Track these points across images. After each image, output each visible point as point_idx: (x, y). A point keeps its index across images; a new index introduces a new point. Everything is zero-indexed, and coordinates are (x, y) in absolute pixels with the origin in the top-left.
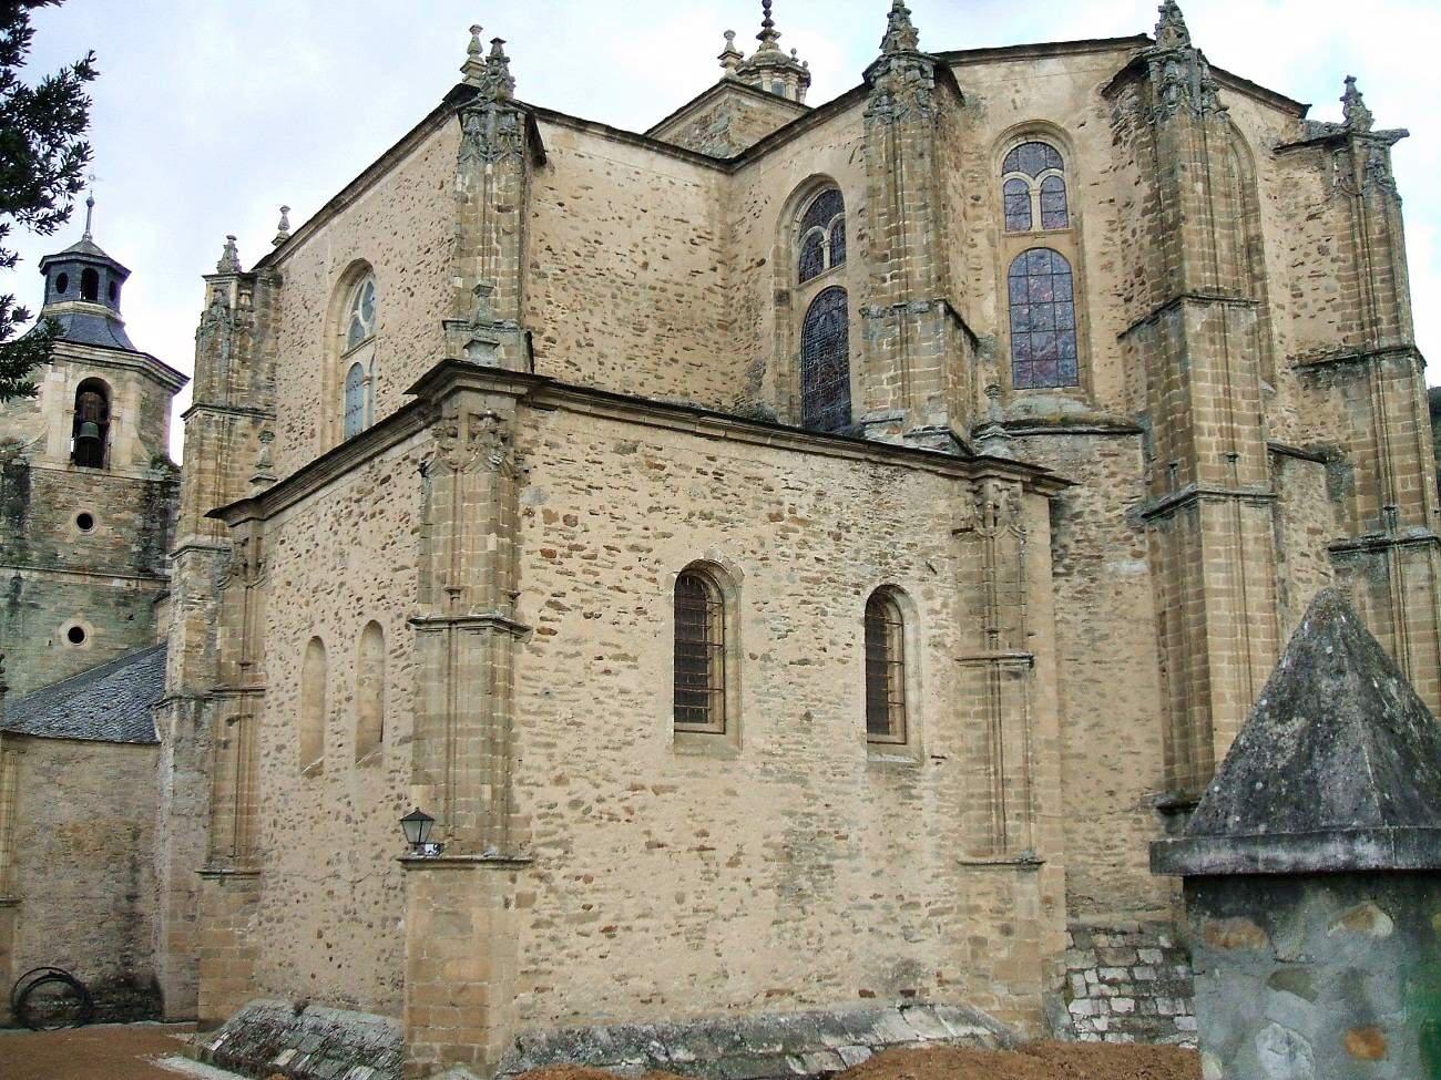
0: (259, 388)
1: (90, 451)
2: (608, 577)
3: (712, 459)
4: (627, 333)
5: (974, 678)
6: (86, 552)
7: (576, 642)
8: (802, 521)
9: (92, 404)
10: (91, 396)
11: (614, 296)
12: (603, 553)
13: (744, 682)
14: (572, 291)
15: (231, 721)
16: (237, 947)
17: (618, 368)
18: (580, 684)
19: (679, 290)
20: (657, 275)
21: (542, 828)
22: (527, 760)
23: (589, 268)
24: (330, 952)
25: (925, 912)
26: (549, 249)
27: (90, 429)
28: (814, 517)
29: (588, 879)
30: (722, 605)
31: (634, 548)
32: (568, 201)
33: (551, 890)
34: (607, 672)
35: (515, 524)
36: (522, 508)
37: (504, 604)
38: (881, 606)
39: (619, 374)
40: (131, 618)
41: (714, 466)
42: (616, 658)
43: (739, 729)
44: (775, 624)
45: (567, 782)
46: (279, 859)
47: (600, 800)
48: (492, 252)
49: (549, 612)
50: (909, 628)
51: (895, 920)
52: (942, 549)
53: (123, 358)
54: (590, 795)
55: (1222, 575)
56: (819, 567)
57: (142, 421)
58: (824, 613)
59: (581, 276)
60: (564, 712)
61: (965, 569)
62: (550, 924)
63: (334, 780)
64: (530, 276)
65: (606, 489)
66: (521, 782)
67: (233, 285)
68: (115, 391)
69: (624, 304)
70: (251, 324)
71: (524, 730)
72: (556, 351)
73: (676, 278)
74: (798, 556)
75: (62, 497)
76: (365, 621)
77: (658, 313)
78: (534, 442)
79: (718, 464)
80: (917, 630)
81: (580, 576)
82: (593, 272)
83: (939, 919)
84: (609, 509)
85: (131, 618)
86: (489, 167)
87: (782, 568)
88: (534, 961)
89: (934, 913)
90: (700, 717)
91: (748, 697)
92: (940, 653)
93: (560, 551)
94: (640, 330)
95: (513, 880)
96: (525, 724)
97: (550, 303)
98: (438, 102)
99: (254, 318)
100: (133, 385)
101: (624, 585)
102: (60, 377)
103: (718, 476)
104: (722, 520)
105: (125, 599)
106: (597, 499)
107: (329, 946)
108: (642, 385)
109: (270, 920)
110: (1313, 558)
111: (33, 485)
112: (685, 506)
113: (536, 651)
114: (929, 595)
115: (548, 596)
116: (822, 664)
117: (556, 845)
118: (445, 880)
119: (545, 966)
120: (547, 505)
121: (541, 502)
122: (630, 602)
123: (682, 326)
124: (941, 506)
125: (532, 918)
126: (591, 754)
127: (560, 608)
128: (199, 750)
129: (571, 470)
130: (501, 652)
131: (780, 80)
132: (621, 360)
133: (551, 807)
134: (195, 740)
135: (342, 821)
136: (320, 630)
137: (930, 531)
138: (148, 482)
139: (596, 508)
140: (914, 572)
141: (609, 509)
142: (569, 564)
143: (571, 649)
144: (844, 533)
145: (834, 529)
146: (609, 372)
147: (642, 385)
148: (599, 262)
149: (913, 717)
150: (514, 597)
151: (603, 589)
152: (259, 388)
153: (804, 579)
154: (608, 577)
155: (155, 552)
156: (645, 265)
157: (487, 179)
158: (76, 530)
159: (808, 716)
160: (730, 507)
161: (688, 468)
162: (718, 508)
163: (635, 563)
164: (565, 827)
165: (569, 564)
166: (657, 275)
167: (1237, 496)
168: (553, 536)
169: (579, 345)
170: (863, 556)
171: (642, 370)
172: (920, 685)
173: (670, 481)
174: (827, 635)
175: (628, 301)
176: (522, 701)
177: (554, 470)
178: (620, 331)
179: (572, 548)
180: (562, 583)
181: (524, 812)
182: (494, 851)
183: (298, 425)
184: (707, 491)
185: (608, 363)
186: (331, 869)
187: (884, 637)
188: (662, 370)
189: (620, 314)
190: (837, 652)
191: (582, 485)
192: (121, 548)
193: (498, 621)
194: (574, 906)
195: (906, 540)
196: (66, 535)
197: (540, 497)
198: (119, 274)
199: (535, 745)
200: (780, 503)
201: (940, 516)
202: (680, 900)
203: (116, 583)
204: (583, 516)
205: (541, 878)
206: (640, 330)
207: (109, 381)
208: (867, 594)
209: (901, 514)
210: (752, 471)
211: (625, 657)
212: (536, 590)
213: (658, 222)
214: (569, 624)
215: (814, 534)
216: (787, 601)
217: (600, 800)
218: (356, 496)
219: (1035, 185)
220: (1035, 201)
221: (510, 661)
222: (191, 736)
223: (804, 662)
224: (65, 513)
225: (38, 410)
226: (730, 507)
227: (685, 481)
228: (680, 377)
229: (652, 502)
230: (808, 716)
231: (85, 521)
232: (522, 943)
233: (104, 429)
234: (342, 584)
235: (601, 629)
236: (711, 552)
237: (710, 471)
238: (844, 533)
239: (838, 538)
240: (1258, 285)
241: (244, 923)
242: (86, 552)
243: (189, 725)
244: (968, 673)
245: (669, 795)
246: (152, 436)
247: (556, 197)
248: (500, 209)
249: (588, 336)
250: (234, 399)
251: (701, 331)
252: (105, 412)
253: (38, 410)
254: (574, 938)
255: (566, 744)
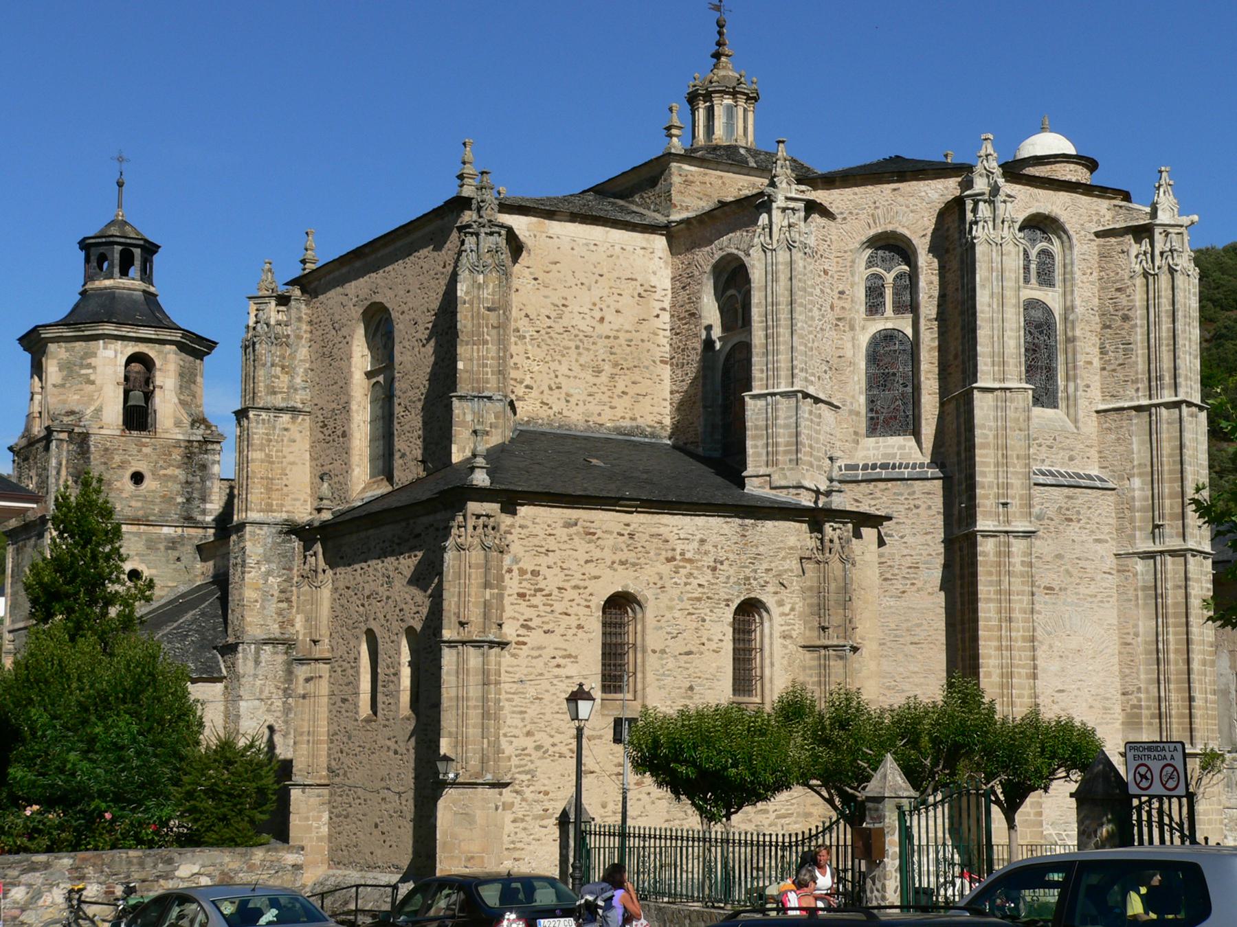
0: (296, 390)
1: (138, 417)
2: (559, 607)
3: (628, 525)
4: (588, 375)
5: (812, 659)
6: (139, 504)
7: (539, 648)
8: (690, 561)
9: (140, 373)
10: (136, 367)
11: (577, 347)
12: (556, 592)
13: (647, 668)
14: (545, 347)
15: (308, 680)
16: (314, 834)
17: (581, 403)
18: (541, 674)
19: (628, 336)
20: (612, 326)
21: (518, 763)
22: (509, 722)
23: (558, 328)
24: (383, 837)
25: (772, 816)
26: (527, 316)
27: (137, 398)
28: (697, 557)
29: (546, 793)
30: (634, 618)
31: (576, 587)
32: (541, 276)
33: (523, 800)
34: (558, 666)
35: (501, 578)
36: (505, 568)
37: (494, 629)
38: (749, 610)
39: (581, 409)
40: (178, 559)
41: (629, 529)
42: (564, 657)
43: (644, 697)
44: (669, 629)
45: (533, 735)
46: (345, 774)
47: (554, 745)
48: (485, 342)
49: (522, 631)
50: (766, 624)
51: (750, 821)
52: (792, 571)
53: (164, 335)
54: (547, 742)
55: (992, 589)
56: (700, 590)
57: (181, 386)
58: (704, 620)
59: (552, 334)
60: (531, 691)
61: (809, 584)
62: (523, 820)
63: (385, 726)
64: (513, 339)
65: (558, 552)
66: (505, 735)
67: (273, 303)
68: (158, 363)
69: (586, 353)
70: (288, 336)
71: (507, 704)
72: (532, 395)
73: (627, 327)
74: (686, 584)
75: (117, 459)
76: (405, 626)
77: (612, 357)
78: (512, 526)
79: (631, 528)
80: (771, 627)
81: (541, 608)
82: (561, 330)
83: (783, 821)
84: (560, 564)
85: (178, 559)
86: (481, 278)
87: (675, 592)
88: (513, 842)
89: (778, 817)
90: (618, 689)
91: (650, 677)
92: (788, 642)
93: (528, 593)
94: (598, 371)
95: (501, 794)
96: (508, 700)
97: (528, 358)
98: (441, 203)
99: (289, 330)
100: (172, 357)
101: (569, 611)
102: (110, 353)
103: (631, 536)
104: (634, 565)
105: (173, 544)
106: (551, 559)
107: (383, 833)
108: (599, 415)
109: (338, 816)
110: (627, 536)
111: (92, 449)
112: (608, 556)
113: (513, 655)
114: (781, 603)
115: (521, 622)
116: (702, 653)
117: (527, 773)
118: (461, 794)
119: (519, 845)
120: (521, 565)
121: (517, 563)
122: (573, 621)
123: (631, 365)
124: (792, 541)
125: (511, 817)
126: (548, 717)
127: (528, 628)
128: (258, 683)
129: (536, 541)
130: (492, 659)
131: (730, 102)
132: (584, 397)
133: (524, 750)
134: (256, 676)
135: (391, 753)
136: (374, 626)
137: (784, 559)
138: (189, 441)
139: (551, 564)
140: (770, 588)
141: (560, 564)
142: (534, 601)
143: (535, 653)
144: (719, 566)
145: (712, 564)
146: (574, 407)
147: (599, 415)
148: (565, 322)
149: (767, 686)
150: (500, 625)
151: (556, 615)
152: (296, 390)
153: (689, 599)
154: (559, 607)
155: (197, 502)
156: (602, 320)
157: (479, 286)
158: (130, 486)
159: (691, 688)
160: (640, 555)
161: (611, 533)
162: (631, 557)
163: (576, 596)
164: (532, 762)
165: (534, 601)
166: (612, 326)
167: (1007, 532)
168: (525, 584)
169: (551, 389)
170: (732, 580)
171: (601, 403)
172: (772, 664)
173: (599, 542)
174: (705, 634)
175: (588, 350)
176: (505, 687)
177: (525, 542)
178: (582, 375)
179: (536, 590)
180: (530, 613)
181: (507, 753)
182: (489, 777)
183: (331, 424)
184: (624, 546)
185: (573, 400)
186: (383, 784)
187: (750, 632)
188: (616, 402)
189: (582, 361)
190: (714, 646)
191: (543, 550)
192: (167, 499)
193: (491, 642)
194: (538, 810)
195: (765, 566)
196: (121, 491)
197: (516, 560)
198: (150, 249)
199: (513, 712)
200: (674, 550)
201: (791, 548)
202: (604, 806)
203: (165, 530)
204: (543, 570)
205: (517, 792)
206: (598, 371)
207: (152, 354)
208: (734, 606)
209: (761, 549)
210: (655, 531)
211: (570, 656)
212: (514, 618)
213: (612, 283)
214: (535, 638)
215: (697, 568)
216: (677, 614)
217: (554, 745)
218: (396, 541)
219: (890, 277)
220: (889, 293)
221: (499, 664)
222: (252, 672)
223: (689, 653)
224: (120, 472)
225: (93, 383)
226: (640, 555)
227: (609, 541)
228: (629, 406)
229: (587, 557)
230: (691, 688)
231: (138, 478)
232: (506, 831)
233: (148, 396)
234: (388, 598)
235: (554, 640)
236: (627, 585)
237: (626, 533)
238: (719, 566)
239: (714, 569)
240: (1070, 346)
241: (320, 818)
242: (139, 504)
243: (251, 664)
244: (808, 655)
245: (597, 741)
246: (189, 399)
247: (531, 273)
248: (489, 309)
249: (557, 381)
250: (278, 401)
251: (647, 368)
252: (148, 380)
253: (93, 383)
254: (537, 829)
255: (533, 711)
